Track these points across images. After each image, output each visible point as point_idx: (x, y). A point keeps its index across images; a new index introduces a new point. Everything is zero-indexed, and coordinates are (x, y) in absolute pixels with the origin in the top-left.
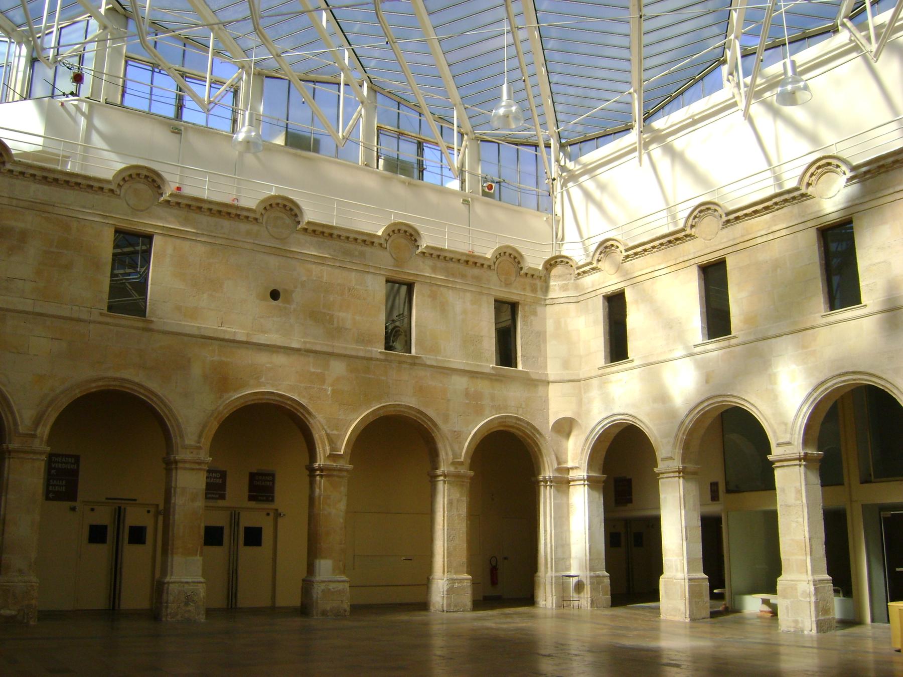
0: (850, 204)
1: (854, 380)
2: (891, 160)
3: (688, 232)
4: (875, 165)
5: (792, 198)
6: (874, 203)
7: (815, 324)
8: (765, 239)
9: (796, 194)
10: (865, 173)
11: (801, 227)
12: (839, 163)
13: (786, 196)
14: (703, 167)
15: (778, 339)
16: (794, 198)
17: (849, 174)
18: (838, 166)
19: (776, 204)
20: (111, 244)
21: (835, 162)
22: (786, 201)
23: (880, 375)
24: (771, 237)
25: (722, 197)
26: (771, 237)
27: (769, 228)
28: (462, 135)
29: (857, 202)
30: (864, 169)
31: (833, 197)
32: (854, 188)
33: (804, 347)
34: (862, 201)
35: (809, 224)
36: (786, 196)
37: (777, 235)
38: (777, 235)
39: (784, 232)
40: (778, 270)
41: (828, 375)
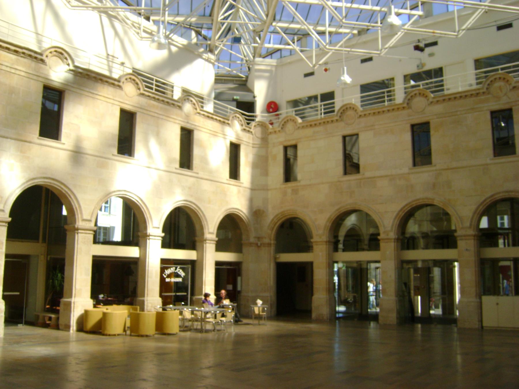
0: (66, 83)
1: (50, 183)
2: (94, 75)
3: (44, 58)
4: (85, 72)
5: (36, 57)
6: (78, 91)
7: (32, 141)
8: (8, 69)
9: (116, 83)
10: (80, 73)
11: (35, 77)
12: (68, 58)
13: (32, 54)
14: (68, 29)
15: (4, 139)
16: (36, 58)
17: (72, 67)
18: (66, 59)
19: (24, 53)
20: (396, 92)
21: (66, 55)
22: (30, 56)
23: (70, 187)
24: (13, 71)
25: (77, 56)
26: (13, 71)
27: (13, 64)
28: (210, 15)
29: (70, 84)
30: (80, 70)
31: (58, 73)
32: (70, 76)
33: (21, 152)
34: (72, 85)
35: (40, 79)
36: (32, 54)
37: (18, 72)
38: (18, 72)
39: (23, 74)
40: (13, 95)
41: (39, 176)
